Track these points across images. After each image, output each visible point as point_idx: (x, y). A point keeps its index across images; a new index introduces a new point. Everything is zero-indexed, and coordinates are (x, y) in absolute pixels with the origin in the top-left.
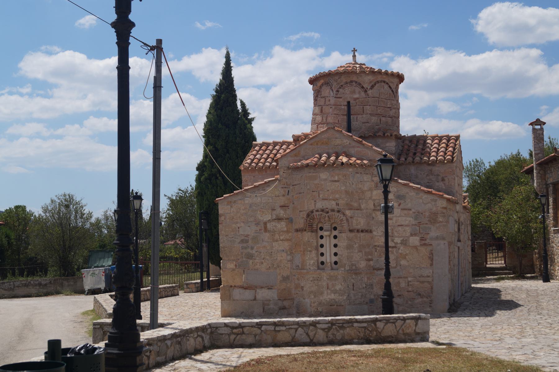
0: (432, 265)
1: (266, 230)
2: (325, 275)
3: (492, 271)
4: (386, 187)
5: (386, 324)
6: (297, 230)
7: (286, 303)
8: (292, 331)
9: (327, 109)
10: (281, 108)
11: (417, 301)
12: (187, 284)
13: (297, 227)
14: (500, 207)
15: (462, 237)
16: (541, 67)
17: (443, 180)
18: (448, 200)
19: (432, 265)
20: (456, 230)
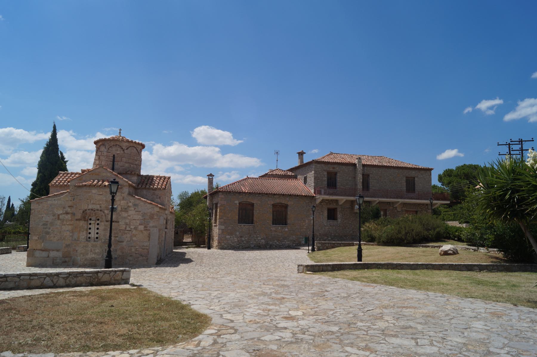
0: (149, 240)
1: (59, 219)
2: (90, 244)
3: (186, 244)
4: (113, 197)
5: (104, 274)
6: (77, 220)
7: (67, 259)
8: (42, 280)
9: (102, 158)
10: (80, 155)
11: (140, 259)
12: (19, 247)
13: (77, 218)
14: (191, 213)
15: (168, 227)
16: (219, 155)
17: (160, 198)
18: (160, 208)
19: (149, 240)
20: (165, 223)
